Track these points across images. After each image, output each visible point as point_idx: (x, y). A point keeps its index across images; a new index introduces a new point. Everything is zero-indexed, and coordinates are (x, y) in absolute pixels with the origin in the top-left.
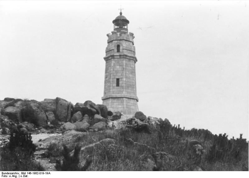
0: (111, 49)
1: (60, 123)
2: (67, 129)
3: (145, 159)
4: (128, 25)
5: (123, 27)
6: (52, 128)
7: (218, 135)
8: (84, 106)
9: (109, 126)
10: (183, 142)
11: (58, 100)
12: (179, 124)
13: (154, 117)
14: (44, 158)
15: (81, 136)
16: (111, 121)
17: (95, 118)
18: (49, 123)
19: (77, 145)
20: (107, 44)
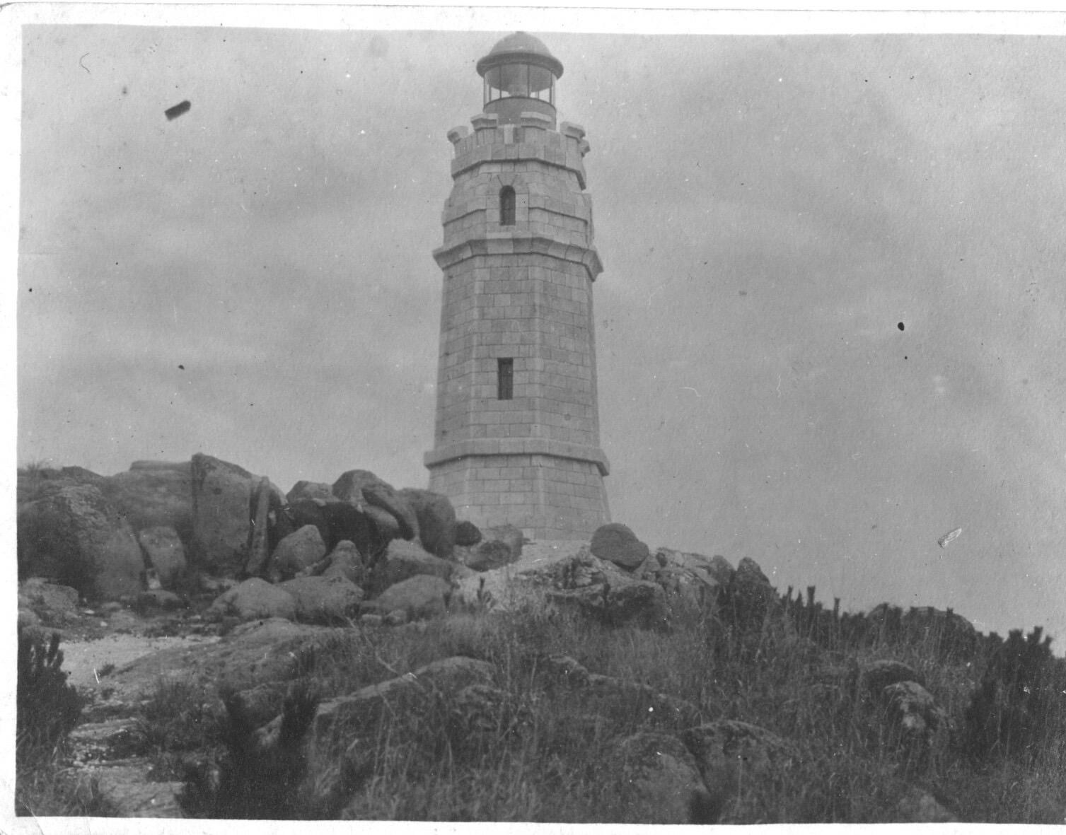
0: (469, 210)
1: (213, 584)
2: (246, 613)
3: (645, 755)
4: (558, 83)
5: (533, 95)
6: (170, 606)
7: (1005, 636)
8: (336, 500)
9: (461, 599)
10: (836, 673)
11: (200, 465)
12: (812, 585)
13: (686, 550)
14: (123, 757)
15: (317, 646)
16: (470, 571)
17: (390, 558)
18: (154, 584)
19: (300, 693)
20: (452, 183)
